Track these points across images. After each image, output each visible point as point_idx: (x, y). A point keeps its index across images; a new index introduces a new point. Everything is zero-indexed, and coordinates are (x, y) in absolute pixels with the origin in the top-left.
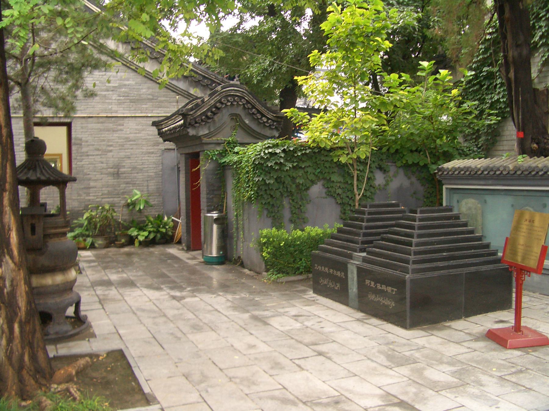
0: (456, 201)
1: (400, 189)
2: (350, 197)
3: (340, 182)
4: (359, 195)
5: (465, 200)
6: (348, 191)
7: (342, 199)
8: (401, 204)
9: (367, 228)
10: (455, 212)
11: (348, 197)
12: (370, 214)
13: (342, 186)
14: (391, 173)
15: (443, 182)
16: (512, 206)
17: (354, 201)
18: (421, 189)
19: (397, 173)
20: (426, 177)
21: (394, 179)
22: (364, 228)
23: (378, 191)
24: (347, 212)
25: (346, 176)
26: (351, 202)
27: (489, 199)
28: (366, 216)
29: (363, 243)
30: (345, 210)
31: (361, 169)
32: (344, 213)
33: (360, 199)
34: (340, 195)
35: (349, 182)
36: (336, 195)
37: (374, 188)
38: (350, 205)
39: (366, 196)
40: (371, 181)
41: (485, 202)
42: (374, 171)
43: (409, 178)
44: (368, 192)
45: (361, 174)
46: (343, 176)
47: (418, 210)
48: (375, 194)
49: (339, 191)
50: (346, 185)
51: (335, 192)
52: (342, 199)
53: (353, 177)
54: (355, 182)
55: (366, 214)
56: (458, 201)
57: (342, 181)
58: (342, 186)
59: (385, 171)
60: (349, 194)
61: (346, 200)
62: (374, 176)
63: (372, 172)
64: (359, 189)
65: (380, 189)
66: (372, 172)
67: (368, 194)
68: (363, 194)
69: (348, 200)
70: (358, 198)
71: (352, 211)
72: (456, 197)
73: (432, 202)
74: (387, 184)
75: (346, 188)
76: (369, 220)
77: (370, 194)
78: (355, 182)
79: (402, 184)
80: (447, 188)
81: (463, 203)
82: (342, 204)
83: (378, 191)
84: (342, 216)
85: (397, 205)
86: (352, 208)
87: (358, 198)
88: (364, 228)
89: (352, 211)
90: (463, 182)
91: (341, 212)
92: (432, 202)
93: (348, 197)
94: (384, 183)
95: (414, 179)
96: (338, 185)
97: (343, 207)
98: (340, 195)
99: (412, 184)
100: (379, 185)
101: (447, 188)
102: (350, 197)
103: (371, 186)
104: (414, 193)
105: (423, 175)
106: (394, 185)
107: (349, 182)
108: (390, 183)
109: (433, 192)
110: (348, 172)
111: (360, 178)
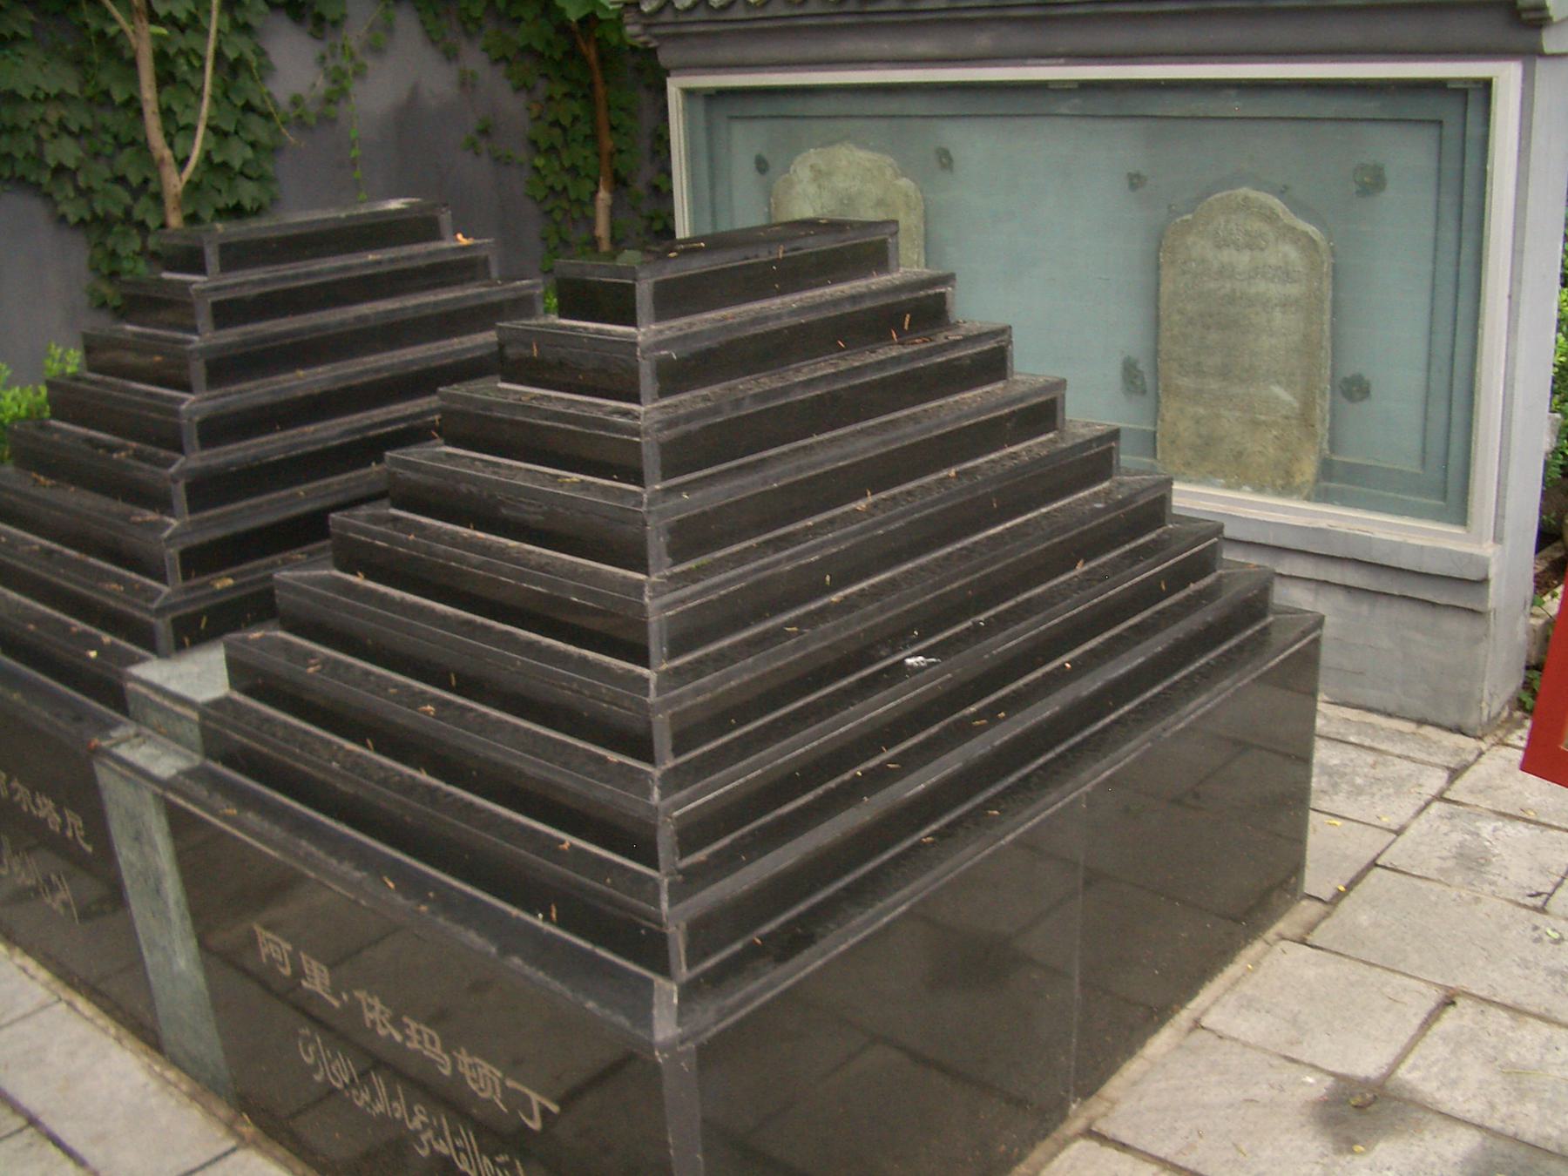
0: (749, 164)
1: (408, 114)
2: (135, 179)
3: (61, 97)
4: (182, 163)
5: (813, 156)
6: (120, 146)
7: (86, 193)
8: (445, 217)
9: (215, 430)
10: (909, 265)
11: (121, 180)
12: (226, 313)
13: (78, 118)
14: (355, 34)
15: (665, 57)
16: (1135, 181)
17: (158, 198)
18: (513, 107)
19: (389, 29)
20: (539, 46)
21: (370, 62)
22: (191, 437)
23: (290, 137)
24: (127, 265)
25: (95, 57)
26: (143, 209)
27: (976, 144)
28: (204, 338)
29: (199, 560)
30: (113, 255)
31: (182, 16)
32: (113, 275)
33: (193, 187)
34: (73, 174)
35: (119, 96)
36: (46, 178)
37: (268, 117)
38: (142, 226)
39: (225, 165)
40: (244, 80)
41: (945, 159)
42: (255, 22)
43: (450, 55)
44: (234, 142)
45: (183, 42)
46: (79, 62)
47: (644, 291)
48: (275, 150)
49: (67, 152)
50: (106, 117)
51: (38, 159)
52: (86, 193)
53: (133, 64)
54: (148, 94)
55: (204, 320)
56: (762, 166)
57: (73, 89)
58: (78, 118)
59: (320, 19)
60: (126, 162)
61: (114, 201)
62: (261, 53)
63: (246, 29)
64: (176, 129)
65: (300, 123)
66: (246, 29)
67: (238, 154)
68: (207, 156)
69: (126, 198)
70: (174, 182)
71: (154, 257)
72: (745, 141)
73: (573, 170)
74: (336, 95)
75: (105, 129)
76: (224, 368)
77: (249, 153)
78: (148, 94)
79: (415, 92)
80: (689, 93)
81: (802, 171)
82: (95, 225)
83: (290, 137)
84: (105, 289)
85: (419, 227)
86: (152, 243)
87: (174, 182)
88: (191, 437)
89: (154, 257)
90: (755, 51)
91: (95, 269)
92: (573, 170)
93: (121, 180)
94: (322, 85)
95: (475, 59)
96: (53, 117)
97: (101, 244)
98: (73, 174)
99: (467, 83)
100: (296, 102)
101: (689, 93)
102: (135, 179)
103: (248, 108)
104: (484, 132)
105: (520, 36)
106: (377, 94)
107: (119, 96)
108: (354, 87)
109: (576, 119)
110: (101, 34)
111: (182, 67)
